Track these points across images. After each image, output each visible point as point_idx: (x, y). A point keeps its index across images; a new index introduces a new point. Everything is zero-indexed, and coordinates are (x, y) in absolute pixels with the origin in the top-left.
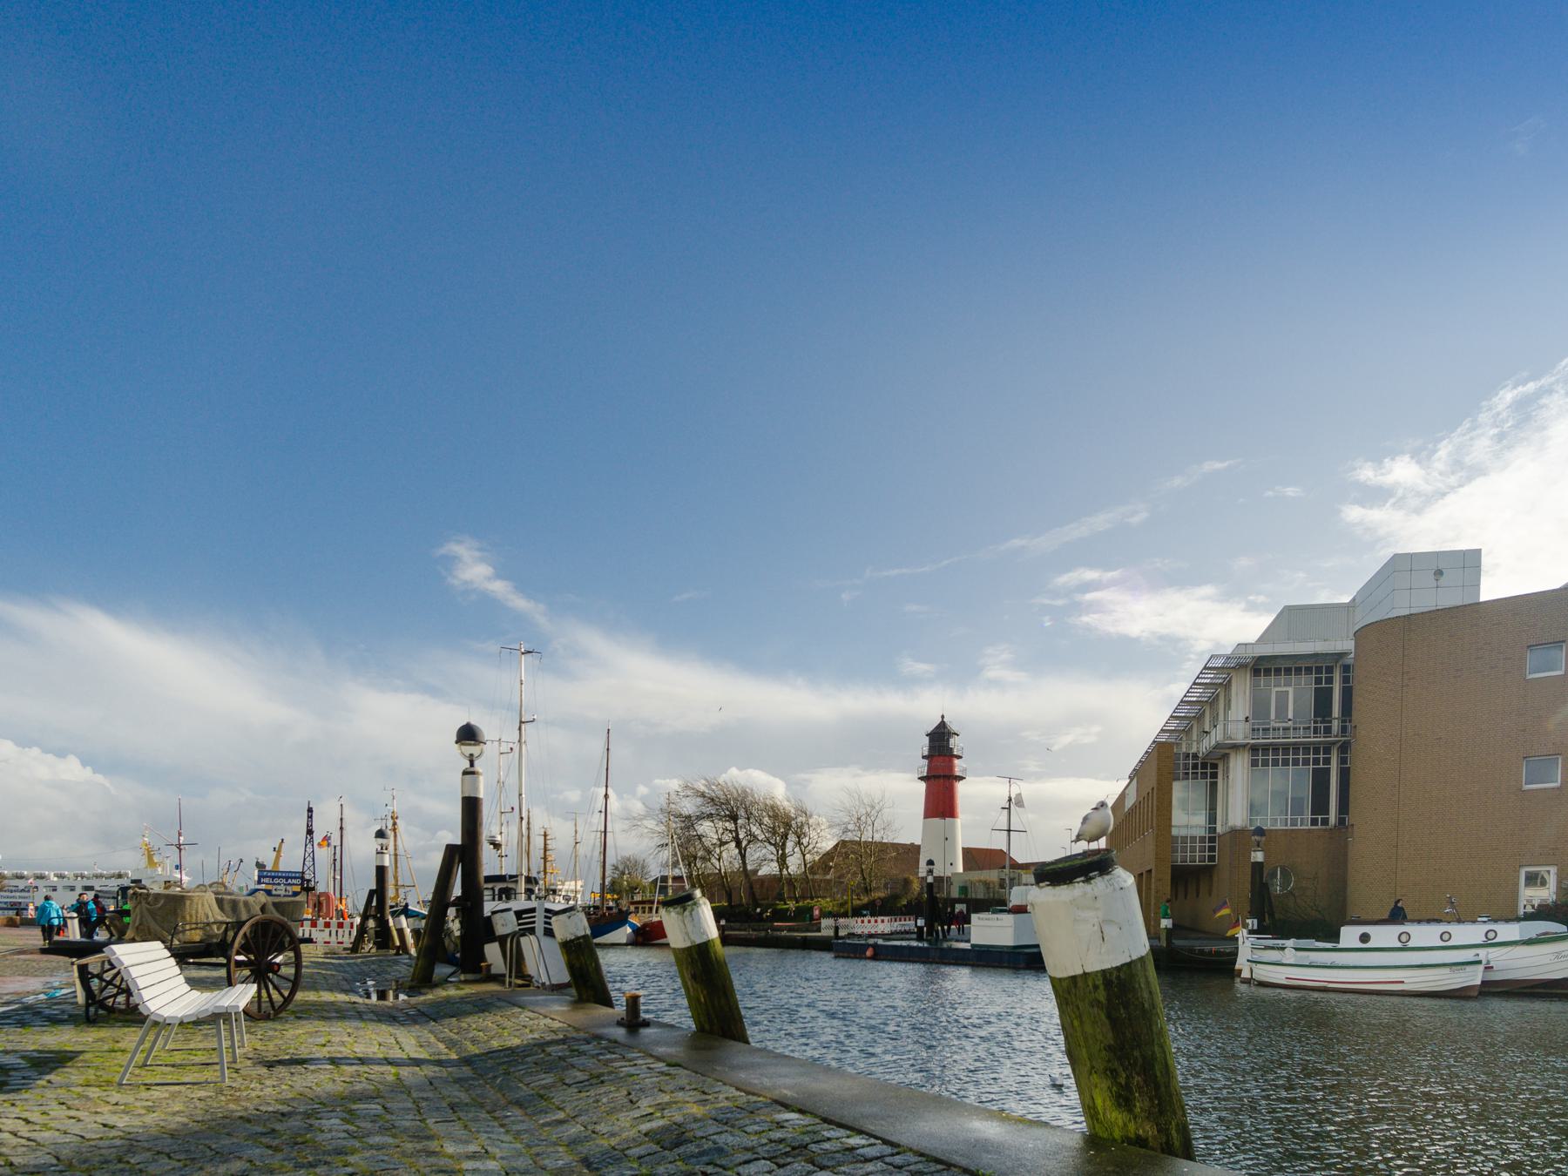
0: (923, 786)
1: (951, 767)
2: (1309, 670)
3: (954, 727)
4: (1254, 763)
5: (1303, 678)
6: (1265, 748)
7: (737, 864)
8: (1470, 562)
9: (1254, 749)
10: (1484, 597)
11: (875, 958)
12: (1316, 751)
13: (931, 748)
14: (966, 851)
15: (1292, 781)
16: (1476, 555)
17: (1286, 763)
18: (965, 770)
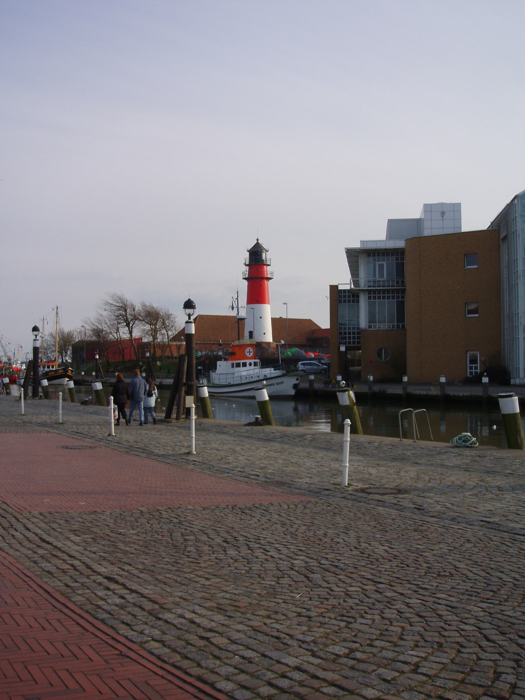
0: (246, 283)
1: (262, 272)
2: (393, 254)
3: (265, 246)
4: (370, 298)
5: (390, 258)
6: (374, 291)
7: (266, 276)
8: (456, 208)
9: (369, 291)
10: (465, 228)
11: (403, 321)
12: (398, 293)
13: (251, 259)
14: (274, 320)
15: (387, 307)
16: (459, 205)
17: (384, 298)
18: (272, 273)
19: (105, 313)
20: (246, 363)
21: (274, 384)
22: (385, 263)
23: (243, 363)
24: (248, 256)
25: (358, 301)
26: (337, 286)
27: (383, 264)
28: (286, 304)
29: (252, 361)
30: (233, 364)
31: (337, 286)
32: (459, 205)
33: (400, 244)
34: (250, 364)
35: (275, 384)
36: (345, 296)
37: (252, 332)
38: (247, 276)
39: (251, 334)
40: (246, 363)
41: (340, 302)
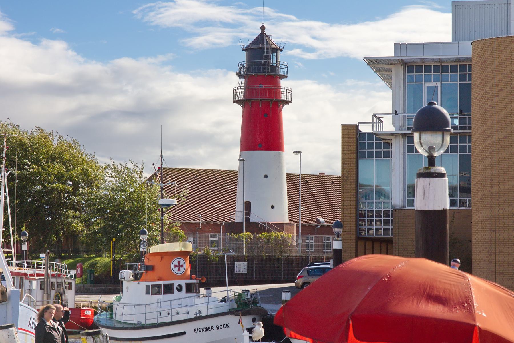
0: (239, 109)
2: (454, 69)
19: (55, 142)
20: (172, 285)
21: (212, 328)
22: (439, 85)
23: (165, 285)
24: (244, 59)
25: (388, 155)
26: (357, 127)
27: (436, 87)
28: (300, 153)
29: (183, 283)
30: (147, 287)
31: (357, 127)
32: (395, 45)
33: (466, 50)
34: (180, 289)
35: (215, 328)
36: (370, 146)
37: (250, 203)
38: (241, 97)
39: (248, 206)
40: (172, 285)
41: (362, 156)
